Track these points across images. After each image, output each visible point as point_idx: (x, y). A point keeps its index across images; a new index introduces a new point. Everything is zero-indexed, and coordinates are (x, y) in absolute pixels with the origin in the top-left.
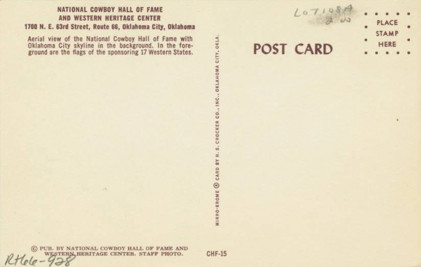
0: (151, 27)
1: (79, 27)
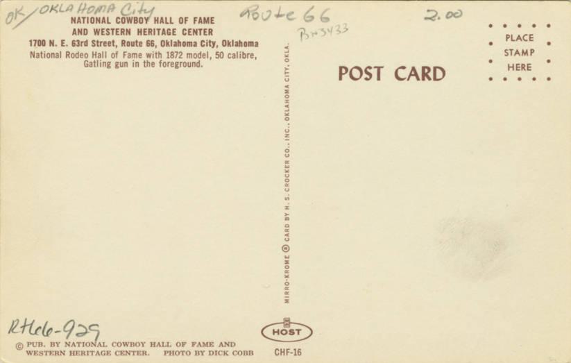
0: (199, 44)
1: (102, 44)
